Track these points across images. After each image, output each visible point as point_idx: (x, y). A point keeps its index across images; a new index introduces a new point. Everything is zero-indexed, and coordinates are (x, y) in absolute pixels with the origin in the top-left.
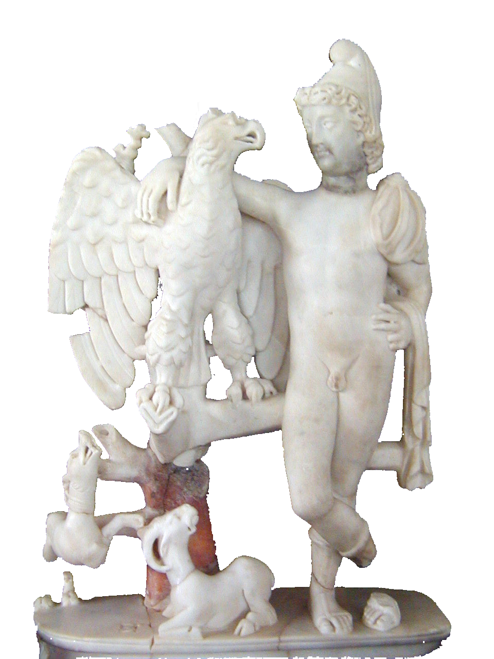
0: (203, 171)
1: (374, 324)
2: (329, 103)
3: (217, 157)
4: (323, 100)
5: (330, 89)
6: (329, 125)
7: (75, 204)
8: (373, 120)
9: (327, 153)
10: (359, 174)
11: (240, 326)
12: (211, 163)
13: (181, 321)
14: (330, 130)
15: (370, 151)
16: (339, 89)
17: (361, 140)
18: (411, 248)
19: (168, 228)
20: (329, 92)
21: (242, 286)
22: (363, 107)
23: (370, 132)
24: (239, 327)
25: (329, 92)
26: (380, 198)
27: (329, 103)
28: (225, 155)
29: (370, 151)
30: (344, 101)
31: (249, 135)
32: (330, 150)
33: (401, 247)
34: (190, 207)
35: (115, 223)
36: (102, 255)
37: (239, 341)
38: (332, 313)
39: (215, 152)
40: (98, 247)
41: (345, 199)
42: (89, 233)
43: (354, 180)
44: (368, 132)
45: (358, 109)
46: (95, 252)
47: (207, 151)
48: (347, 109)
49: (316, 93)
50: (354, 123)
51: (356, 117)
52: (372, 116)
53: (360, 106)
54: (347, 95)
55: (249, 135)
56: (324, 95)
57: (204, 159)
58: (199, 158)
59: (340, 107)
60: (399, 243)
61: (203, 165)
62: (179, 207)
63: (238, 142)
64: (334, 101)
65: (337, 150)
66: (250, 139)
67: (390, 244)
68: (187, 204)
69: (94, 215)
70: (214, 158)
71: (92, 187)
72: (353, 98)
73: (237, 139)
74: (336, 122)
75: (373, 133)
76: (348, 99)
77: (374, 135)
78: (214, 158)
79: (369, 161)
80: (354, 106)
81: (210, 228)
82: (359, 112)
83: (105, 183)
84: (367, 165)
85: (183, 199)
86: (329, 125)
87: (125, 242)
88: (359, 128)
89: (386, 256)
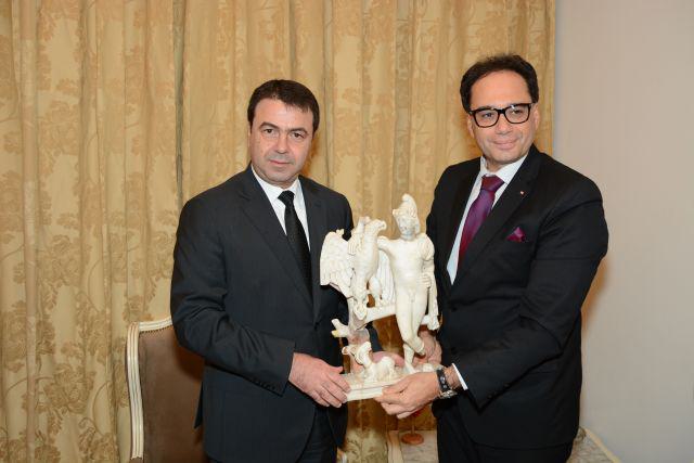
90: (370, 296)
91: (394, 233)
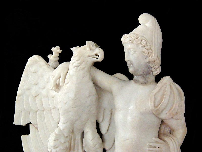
3: (80, 64)
4: (130, 41)
5: (134, 36)
6: (132, 53)
7: (28, 79)
10: (148, 76)
12: (78, 66)
13: (64, 135)
15: (153, 65)
17: (147, 60)
18: (170, 113)
19: (60, 93)
21: (100, 121)
22: (148, 45)
23: (152, 57)
24: (93, 140)
25: (133, 37)
26: (157, 87)
27: (132, 42)
29: (153, 65)
30: (139, 42)
31: (96, 55)
32: (132, 64)
33: (165, 112)
34: (68, 85)
35: (44, 88)
37: (92, 146)
38: (128, 140)
39: (79, 62)
40: (36, 98)
41: (141, 87)
42: (33, 92)
43: (145, 78)
44: (151, 57)
45: (146, 46)
47: (76, 61)
48: (141, 46)
50: (144, 52)
51: (144, 50)
52: (153, 50)
53: (147, 44)
54: (141, 39)
55: (96, 55)
56: (130, 39)
57: (75, 64)
60: (163, 110)
61: (74, 67)
63: (90, 57)
64: (135, 42)
65: (135, 64)
66: (97, 57)
67: (157, 110)
68: (67, 84)
69: (36, 84)
71: (35, 72)
72: (143, 41)
73: (89, 56)
74: (135, 52)
75: (153, 57)
76: (141, 41)
77: (153, 59)
79: (153, 70)
81: (76, 96)
83: (40, 71)
84: (152, 71)
85: (66, 82)
86: (132, 53)
87: (47, 97)
88: (146, 55)
89: (156, 115)
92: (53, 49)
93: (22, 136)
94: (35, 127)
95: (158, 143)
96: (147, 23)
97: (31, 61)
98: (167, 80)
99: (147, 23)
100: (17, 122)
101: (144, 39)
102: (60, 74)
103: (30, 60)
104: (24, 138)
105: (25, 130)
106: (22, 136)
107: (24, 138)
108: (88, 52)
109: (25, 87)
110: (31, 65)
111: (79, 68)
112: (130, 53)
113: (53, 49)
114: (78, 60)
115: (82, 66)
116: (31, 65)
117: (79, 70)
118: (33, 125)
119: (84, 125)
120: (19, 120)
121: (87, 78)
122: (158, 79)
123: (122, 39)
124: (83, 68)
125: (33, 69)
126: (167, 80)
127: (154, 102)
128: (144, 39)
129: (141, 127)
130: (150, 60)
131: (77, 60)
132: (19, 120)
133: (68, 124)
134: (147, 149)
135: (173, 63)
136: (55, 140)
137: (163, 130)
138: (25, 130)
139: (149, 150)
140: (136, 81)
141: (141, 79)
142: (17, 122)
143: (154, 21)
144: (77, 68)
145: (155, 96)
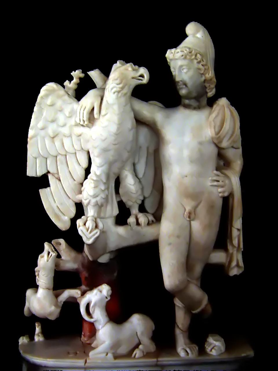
0: (114, 96)
1: (211, 183)
2: (185, 58)
3: (122, 88)
5: (186, 50)
6: (185, 71)
8: (210, 68)
9: (184, 86)
11: (135, 184)
12: (119, 92)
13: (101, 180)
14: (186, 73)
16: (191, 50)
17: (203, 78)
20: (185, 52)
21: (136, 161)
22: (204, 60)
23: (208, 75)
28: (126, 87)
30: (193, 57)
35: (64, 125)
36: (57, 143)
38: (186, 176)
39: (121, 86)
40: (55, 139)
45: (202, 61)
46: (53, 142)
48: (195, 61)
49: (178, 52)
50: (199, 69)
51: (200, 66)
54: (195, 54)
56: (182, 53)
57: (115, 90)
58: (112, 89)
59: (191, 60)
60: (224, 137)
61: (114, 93)
62: (101, 117)
64: (188, 57)
65: (190, 84)
67: (219, 137)
68: (105, 115)
69: (53, 121)
70: (121, 89)
71: (52, 105)
72: (198, 56)
73: (133, 78)
74: (189, 69)
77: (210, 76)
78: (121, 89)
79: (208, 91)
80: (199, 60)
81: (118, 129)
82: (202, 63)
83: (59, 103)
85: (103, 112)
86: (185, 71)
88: (202, 72)
90: (121, 205)
91: (161, 90)
92: (73, 74)
93: (40, 190)
94: (55, 177)
95: (218, 176)
96: (196, 34)
97: (47, 90)
98: (223, 101)
99: (196, 34)
100: (30, 172)
101: (191, 54)
102: (93, 103)
103: (43, 91)
104: (43, 193)
105: (43, 181)
106: (40, 190)
107: (43, 193)
108: (124, 74)
109: (40, 125)
110: (47, 96)
111: (120, 94)
112: (182, 72)
113: (73, 74)
114: (119, 84)
115: (125, 91)
116: (47, 96)
117: (120, 97)
118: (53, 175)
119: (122, 168)
120: (34, 169)
121: (128, 108)
122: (211, 102)
123: (167, 55)
124: (125, 94)
125: (49, 101)
126: (223, 101)
127: (215, 128)
128: (191, 54)
129: (199, 160)
130: (207, 79)
131: (119, 83)
132: (34, 169)
133: (105, 168)
134: (210, 184)
135: (229, 80)
136: (95, 187)
137: (222, 161)
138: (43, 181)
139: (212, 186)
140: (187, 107)
141: (193, 103)
142: (30, 172)
143: (206, 34)
144: (117, 95)
145: (214, 121)
